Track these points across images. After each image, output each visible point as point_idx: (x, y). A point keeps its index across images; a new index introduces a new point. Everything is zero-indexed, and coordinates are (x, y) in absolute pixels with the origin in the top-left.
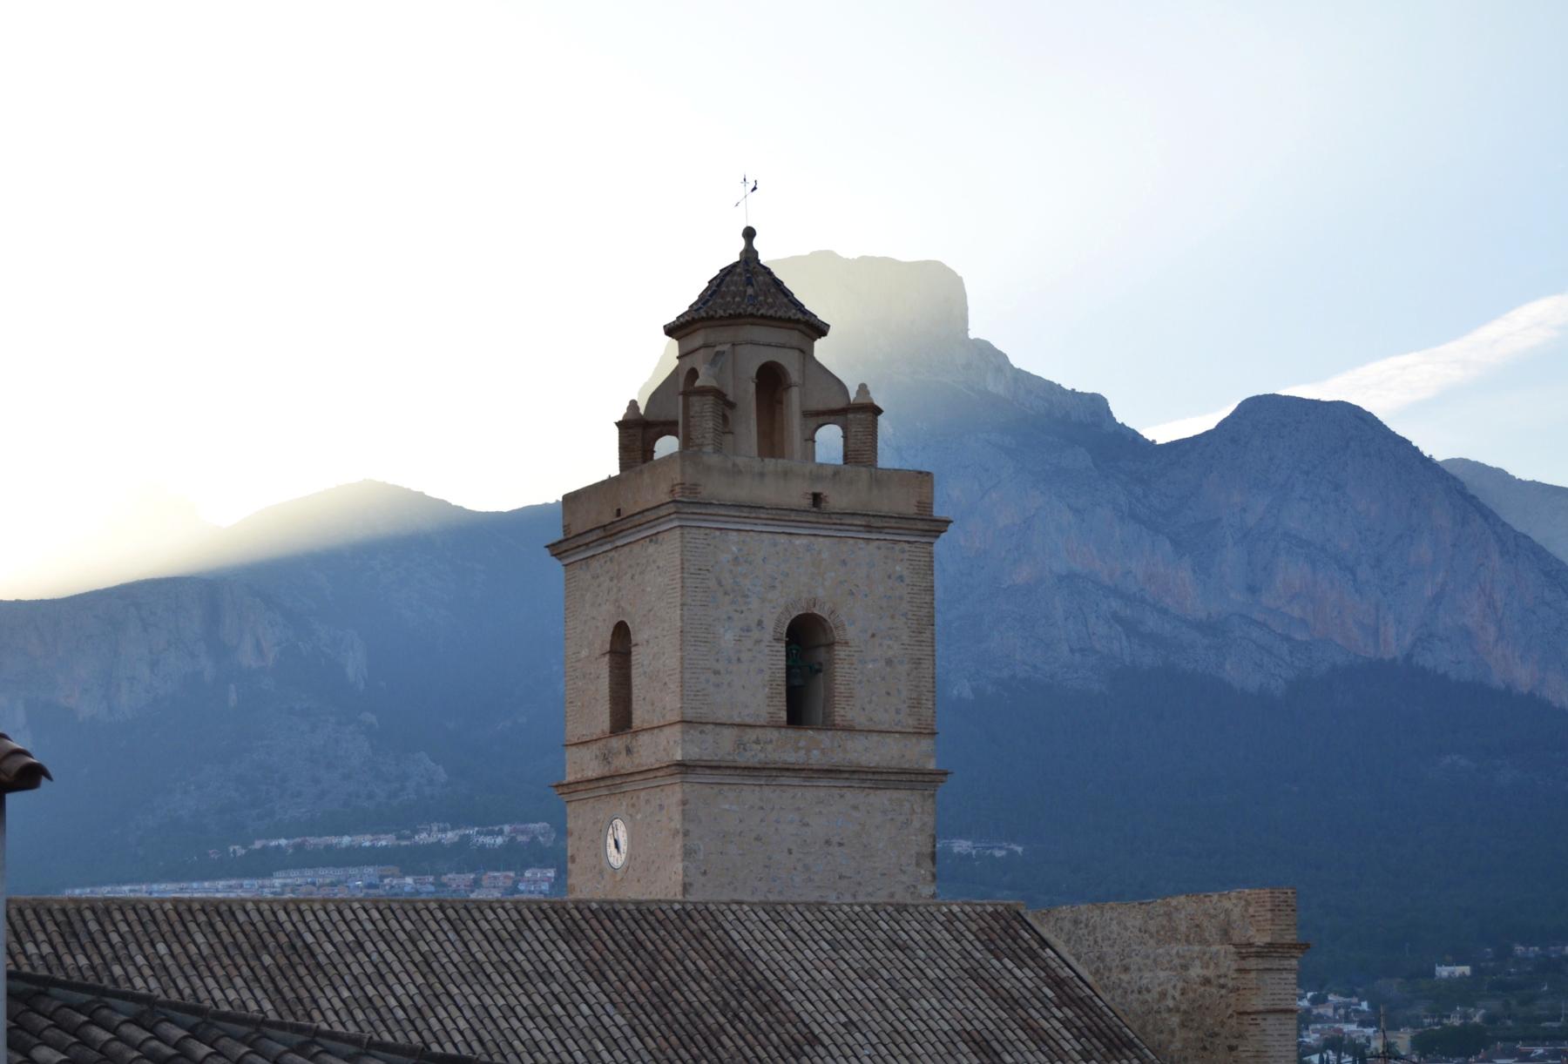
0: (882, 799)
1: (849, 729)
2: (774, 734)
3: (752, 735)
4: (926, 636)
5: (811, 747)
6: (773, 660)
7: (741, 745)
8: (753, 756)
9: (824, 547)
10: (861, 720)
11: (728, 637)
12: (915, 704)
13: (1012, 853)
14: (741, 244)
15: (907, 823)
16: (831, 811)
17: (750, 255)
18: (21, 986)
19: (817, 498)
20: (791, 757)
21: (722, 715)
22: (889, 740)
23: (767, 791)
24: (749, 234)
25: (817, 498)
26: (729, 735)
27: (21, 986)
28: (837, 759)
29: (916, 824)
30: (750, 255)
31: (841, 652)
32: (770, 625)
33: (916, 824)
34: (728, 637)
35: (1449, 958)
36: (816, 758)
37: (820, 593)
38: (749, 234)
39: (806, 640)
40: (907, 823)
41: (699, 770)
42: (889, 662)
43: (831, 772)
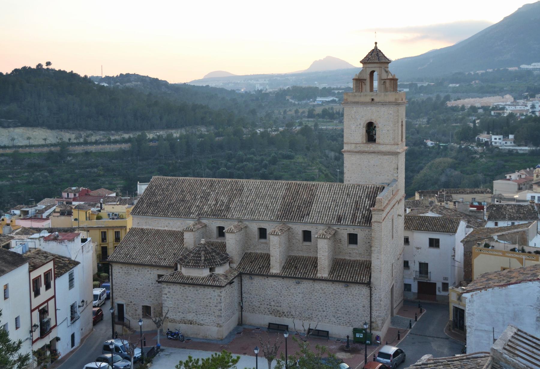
0: (386, 157)
1: (379, 144)
2: (362, 145)
3: (358, 145)
4: (397, 125)
5: (372, 147)
6: (362, 131)
7: (356, 147)
8: (359, 149)
9: (374, 109)
10: (381, 142)
11: (353, 127)
12: (394, 139)
13: (130, 137)
14: (375, 45)
15: (392, 162)
16: (374, 160)
17: (376, 47)
18: (115, 337)
19: (373, 100)
20: (366, 149)
21: (352, 142)
22: (388, 146)
23: (361, 156)
24: (376, 43)
25: (373, 100)
26: (353, 146)
27: (115, 337)
28: (376, 150)
29: (394, 162)
30: (376, 47)
31: (377, 129)
32: (362, 124)
33: (394, 162)
34: (353, 127)
35: (19, 124)
36: (372, 149)
37: (373, 118)
38: (376, 43)
39: (370, 128)
40: (392, 162)
41: (364, 154)
42: (388, 131)
43: (374, 152)
